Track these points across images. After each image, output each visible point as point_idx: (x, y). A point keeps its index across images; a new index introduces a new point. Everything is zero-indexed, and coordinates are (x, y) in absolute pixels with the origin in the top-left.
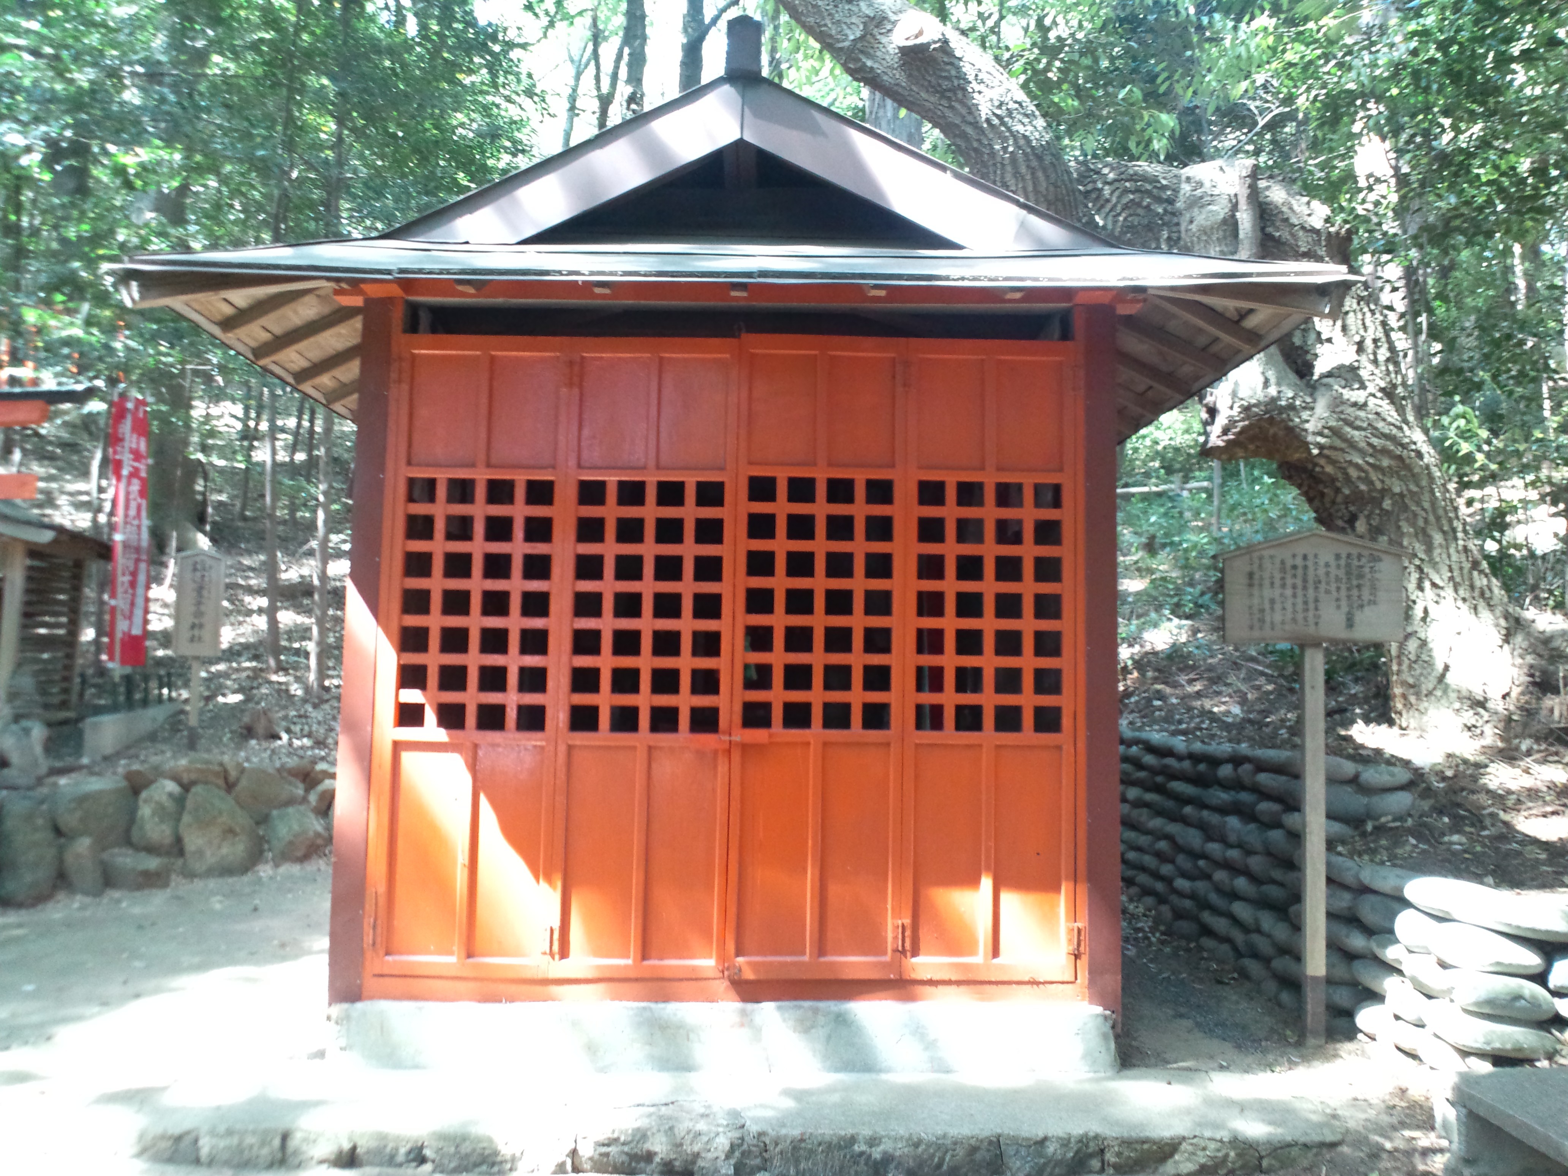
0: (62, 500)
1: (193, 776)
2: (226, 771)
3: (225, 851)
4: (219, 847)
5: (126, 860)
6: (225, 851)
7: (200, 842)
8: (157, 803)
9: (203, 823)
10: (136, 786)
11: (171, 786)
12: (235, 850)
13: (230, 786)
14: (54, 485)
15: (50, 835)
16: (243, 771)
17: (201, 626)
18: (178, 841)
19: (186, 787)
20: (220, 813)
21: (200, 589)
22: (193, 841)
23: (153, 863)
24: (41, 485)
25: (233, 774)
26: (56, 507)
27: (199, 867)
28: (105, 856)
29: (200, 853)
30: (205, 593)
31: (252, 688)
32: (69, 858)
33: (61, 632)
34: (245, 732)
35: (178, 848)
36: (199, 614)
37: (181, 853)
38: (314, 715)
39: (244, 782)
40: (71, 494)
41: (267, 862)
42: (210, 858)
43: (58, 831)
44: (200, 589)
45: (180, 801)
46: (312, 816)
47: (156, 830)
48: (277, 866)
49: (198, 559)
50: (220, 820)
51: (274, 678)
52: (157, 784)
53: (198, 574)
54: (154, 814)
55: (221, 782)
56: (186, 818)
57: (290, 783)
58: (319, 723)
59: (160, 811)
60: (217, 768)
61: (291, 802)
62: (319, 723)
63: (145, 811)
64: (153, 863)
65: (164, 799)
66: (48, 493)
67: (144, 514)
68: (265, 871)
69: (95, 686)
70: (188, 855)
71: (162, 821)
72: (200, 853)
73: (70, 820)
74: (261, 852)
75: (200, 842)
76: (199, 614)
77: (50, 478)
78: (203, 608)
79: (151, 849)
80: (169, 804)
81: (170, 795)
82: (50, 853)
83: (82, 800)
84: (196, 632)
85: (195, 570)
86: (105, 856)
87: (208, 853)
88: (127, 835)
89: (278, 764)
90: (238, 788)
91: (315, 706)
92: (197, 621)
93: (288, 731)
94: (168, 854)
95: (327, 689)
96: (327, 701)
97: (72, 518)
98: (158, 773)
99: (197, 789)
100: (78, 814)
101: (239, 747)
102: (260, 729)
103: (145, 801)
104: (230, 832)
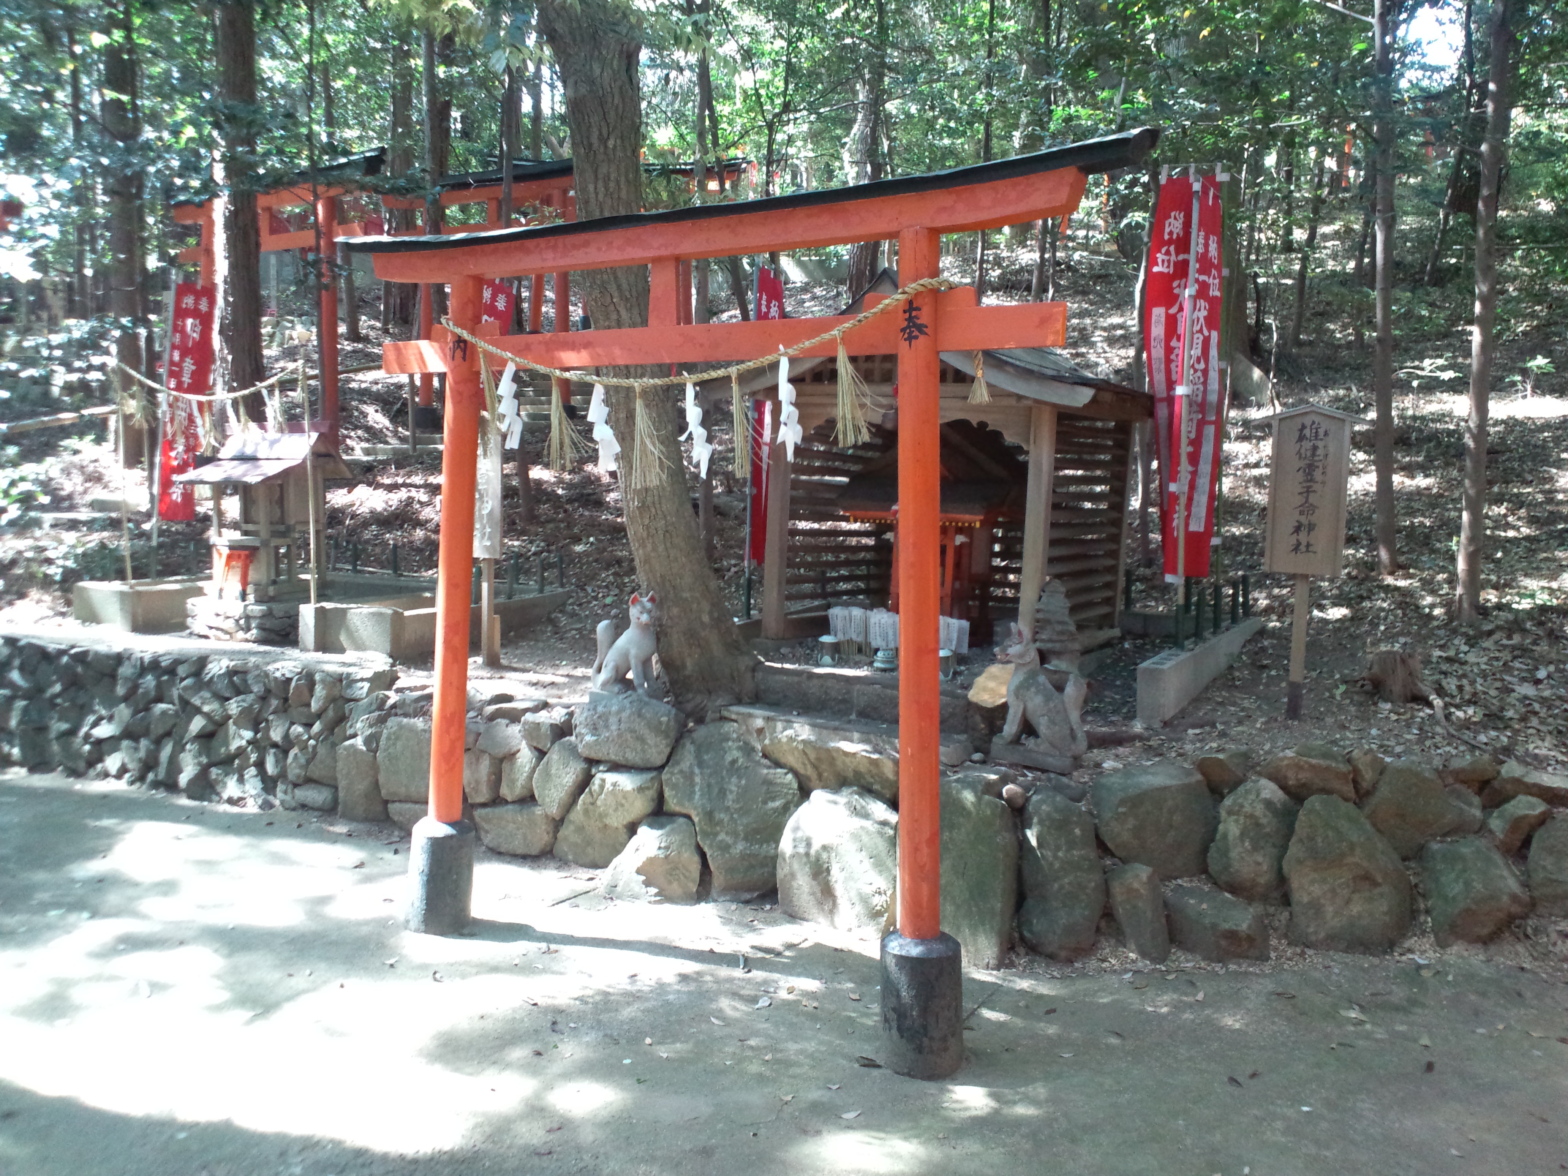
0: (1098, 337)
1: (1304, 776)
2: (1356, 771)
3: (1356, 908)
4: (1348, 902)
5: (1201, 903)
6: (1356, 908)
7: (1316, 890)
8: (1251, 816)
9: (1323, 860)
10: (1216, 783)
11: (1269, 790)
12: (1371, 909)
13: (1361, 795)
14: (1088, 321)
15: (1092, 853)
16: (1382, 769)
17: (1311, 527)
18: (1282, 880)
19: (1297, 795)
20: (1352, 847)
21: (1310, 469)
22: (1306, 886)
23: (1242, 918)
24: (1075, 321)
25: (1368, 775)
26: (1092, 345)
27: (1313, 930)
28: (1168, 890)
29: (1316, 907)
30: (1318, 475)
31: (1362, 598)
32: (1117, 889)
33: (1103, 506)
34: (1369, 687)
35: (1280, 891)
36: (1307, 508)
37: (1286, 900)
38: (1471, 658)
39: (1384, 791)
40: (1104, 329)
41: (1424, 933)
42: (1333, 918)
43: (1102, 846)
44: (1310, 469)
45: (1287, 817)
46: (1497, 857)
47: (1249, 862)
48: (1442, 944)
49: (1307, 421)
50: (1350, 860)
51: (1389, 580)
52: (1249, 785)
53: (1307, 445)
54: (1243, 835)
55: (1349, 790)
56: (1294, 849)
57: (1459, 796)
58: (1484, 675)
59: (1252, 829)
60: (1344, 768)
61: (1460, 829)
62: (1484, 675)
63: (1231, 827)
64: (1242, 918)
65: (1259, 810)
66: (1082, 330)
67: (1214, 352)
68: (1422, 952)
69: (1143, 579)
70: (1296, 908)
71: (1255, 848)
72: (1316, 907)
73: (1120, 832)
74: (1414, 914)
75: (1316, 890)
76: (1307, 508)
77: (1082, 314)
78: (1312, 499)
79: (1238, 889)
80: (1266, 819)
81: (1268, 803)
82: (1093, 881)
83: (1137, 801)
84: (1303, 537)
85: (1301, 438)
86: (1168, 890)
87: (1330, 909)
88: (1201, 856)
89: (1437, 762)
90: (1374, 800)
91: (1472, 642)
92: (1303, 519)
93: (1441, 691)
94: (1265, 899)
95: (1484, 611)
96: (1490, 633)
97: (1108, 360)
98: (1250, 764)
99: (1314, 802)
100: (1131, 823)
101: (1365, 718)
102: (1397, 687)
103: (1230, 813)
104: (1366, 879)
